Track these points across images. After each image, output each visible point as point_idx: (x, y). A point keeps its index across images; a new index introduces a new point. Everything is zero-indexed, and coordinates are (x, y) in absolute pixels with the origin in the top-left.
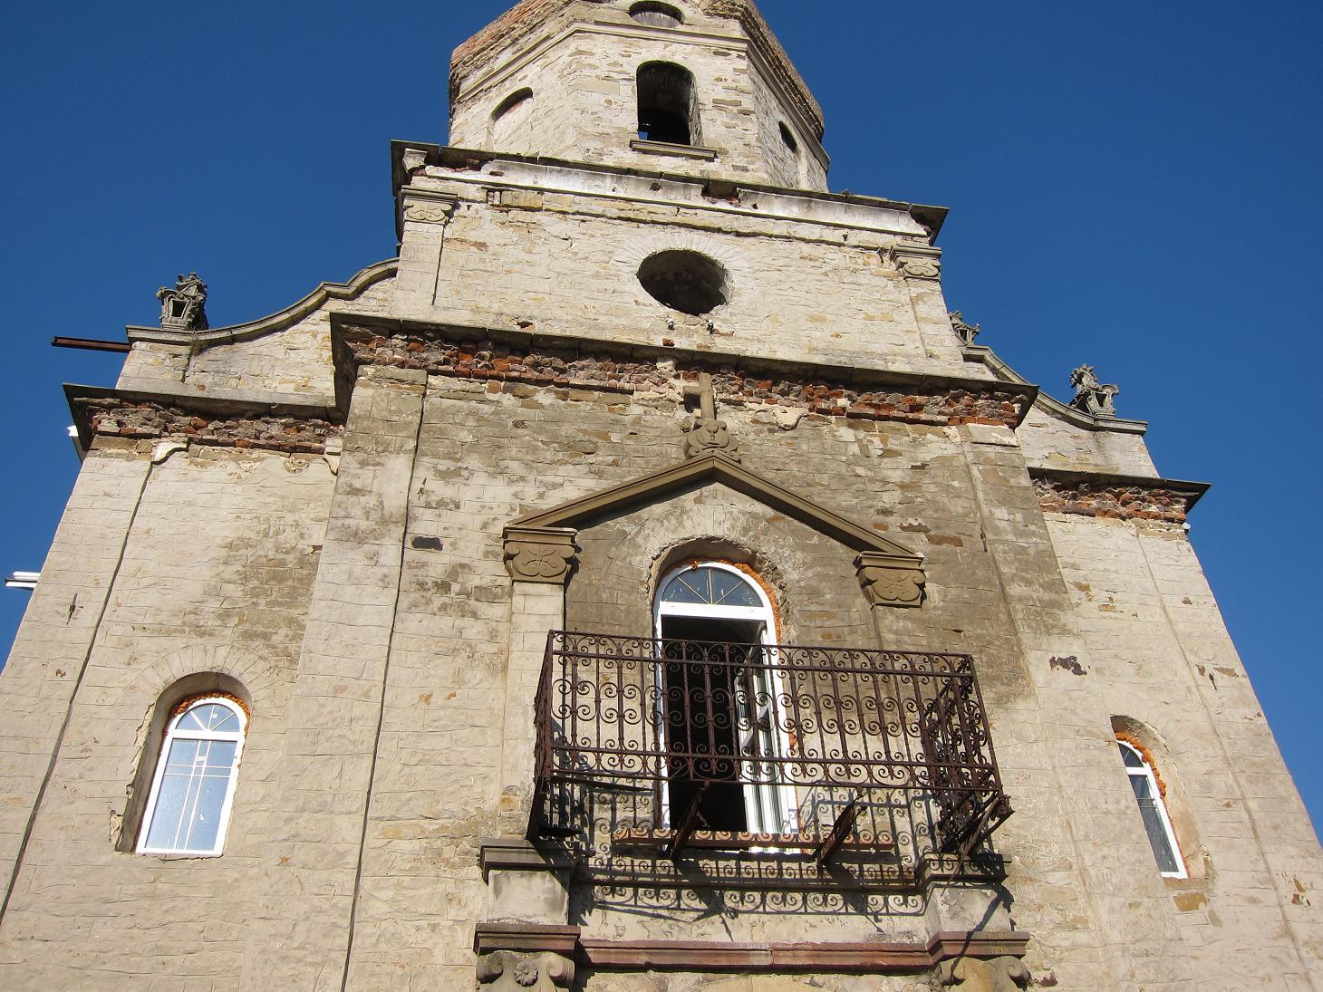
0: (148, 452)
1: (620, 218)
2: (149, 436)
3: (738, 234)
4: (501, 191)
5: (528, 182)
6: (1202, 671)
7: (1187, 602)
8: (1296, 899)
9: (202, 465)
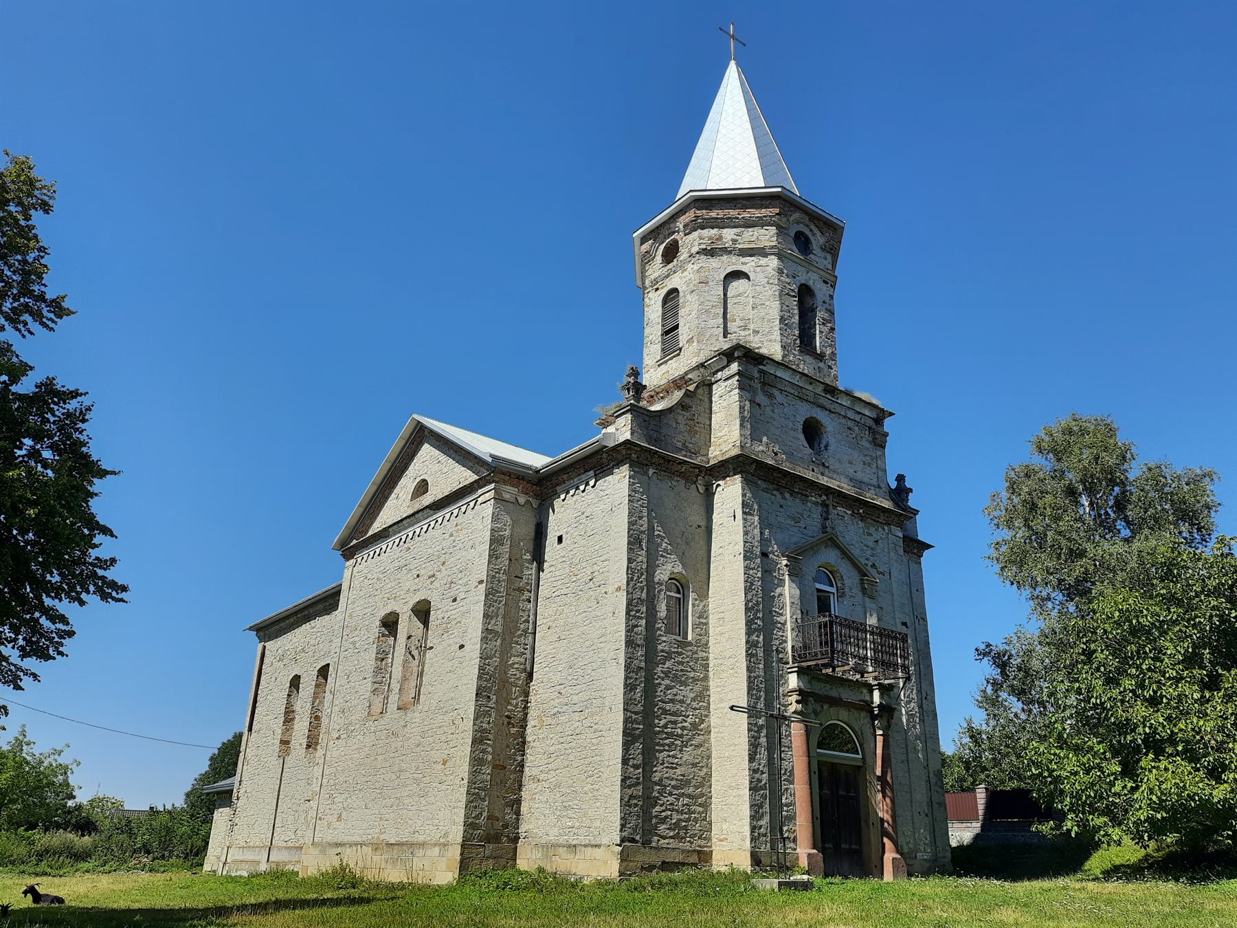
0: (646, 473)
1: (797, 396)
2: (647, 465)
3: (830, 411)
4: (764, 374)
5: (772, 372)
6: (917, 617)
7: (917, 590)
8: (926, 698)
9: (661, 480)
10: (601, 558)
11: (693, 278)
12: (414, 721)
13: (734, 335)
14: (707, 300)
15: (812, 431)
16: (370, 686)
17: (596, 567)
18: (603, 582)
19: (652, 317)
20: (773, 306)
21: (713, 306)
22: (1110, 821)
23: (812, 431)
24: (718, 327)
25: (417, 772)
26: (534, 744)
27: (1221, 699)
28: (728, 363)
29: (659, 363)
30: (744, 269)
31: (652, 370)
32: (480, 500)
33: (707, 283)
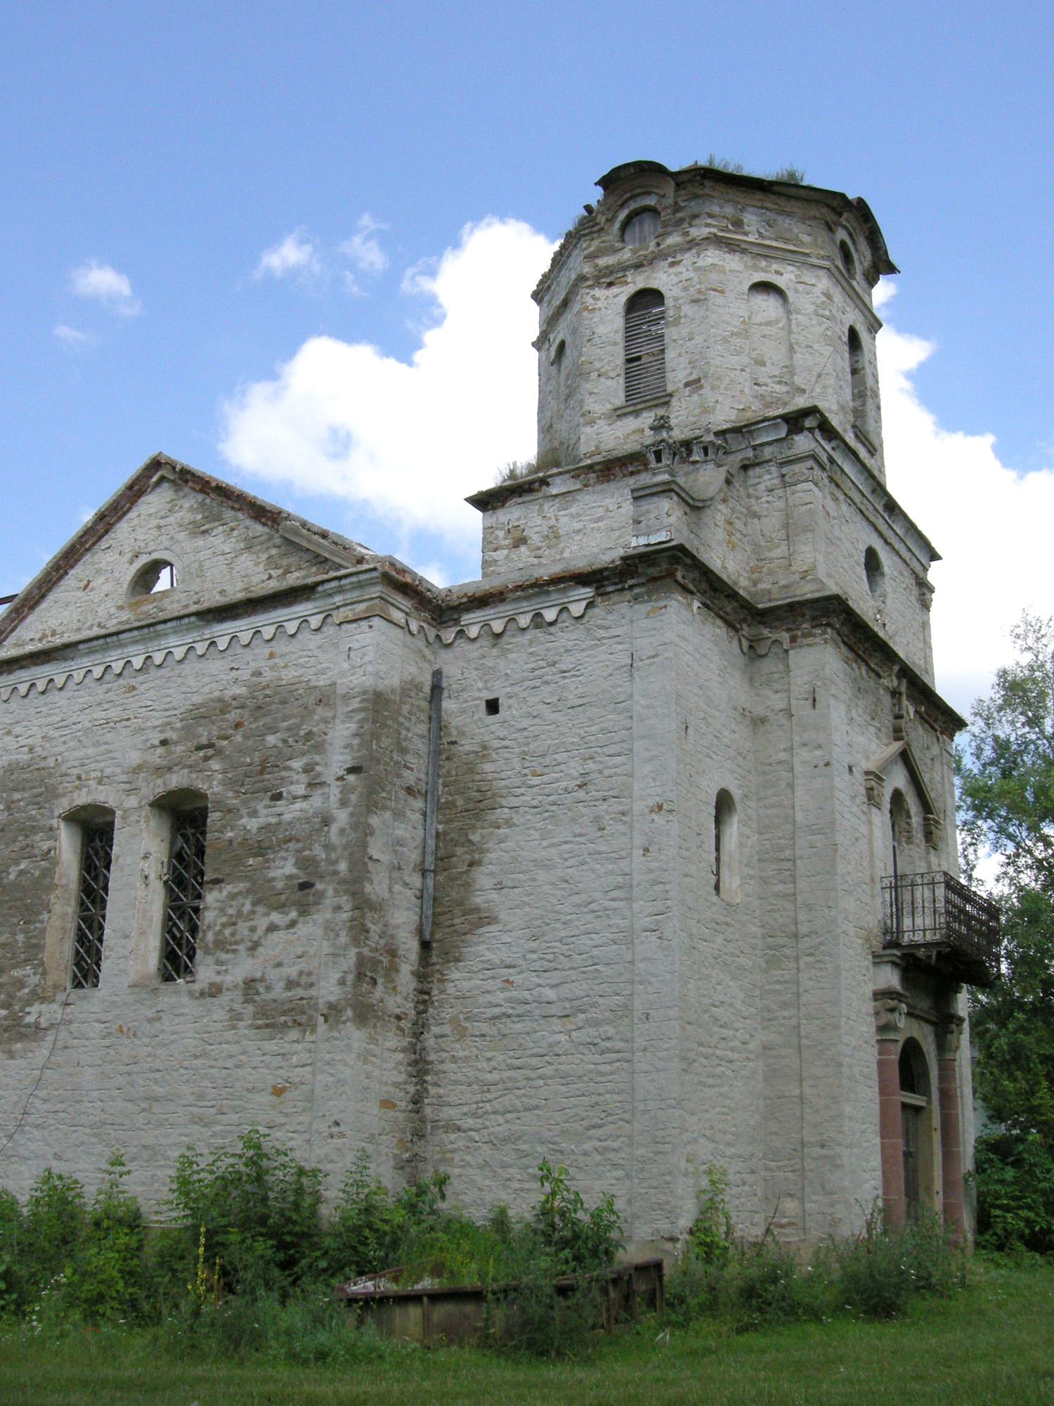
5: (840, 463)
10: (604, 749)
11: (696, 279)
12: (181, 1011)
13: (765, 388)
14: (724, 322)
15: (872, 563)
16: (812, 1328)
17: (591, 765)
18: (612, 793)
19: (601, 330)
20: (825, 353)
21: (733, 334)
22: (985, 1068)
23: (872, 563)
24: (742, 370)
25: (200, 1103)
26: (445, 1067)
27: (402, 737)
28: (787, 435)
29: (619, 412)
30: (780, 282)
31: (601, 422)
32: (338, 616)
33: (722, 292)
